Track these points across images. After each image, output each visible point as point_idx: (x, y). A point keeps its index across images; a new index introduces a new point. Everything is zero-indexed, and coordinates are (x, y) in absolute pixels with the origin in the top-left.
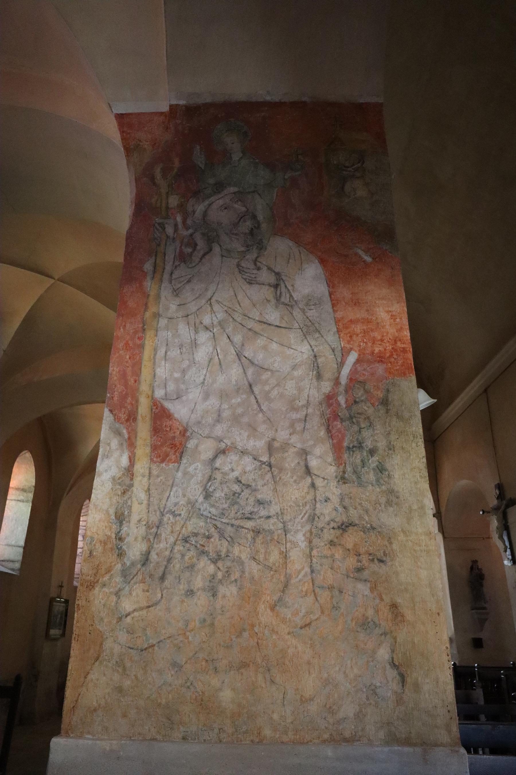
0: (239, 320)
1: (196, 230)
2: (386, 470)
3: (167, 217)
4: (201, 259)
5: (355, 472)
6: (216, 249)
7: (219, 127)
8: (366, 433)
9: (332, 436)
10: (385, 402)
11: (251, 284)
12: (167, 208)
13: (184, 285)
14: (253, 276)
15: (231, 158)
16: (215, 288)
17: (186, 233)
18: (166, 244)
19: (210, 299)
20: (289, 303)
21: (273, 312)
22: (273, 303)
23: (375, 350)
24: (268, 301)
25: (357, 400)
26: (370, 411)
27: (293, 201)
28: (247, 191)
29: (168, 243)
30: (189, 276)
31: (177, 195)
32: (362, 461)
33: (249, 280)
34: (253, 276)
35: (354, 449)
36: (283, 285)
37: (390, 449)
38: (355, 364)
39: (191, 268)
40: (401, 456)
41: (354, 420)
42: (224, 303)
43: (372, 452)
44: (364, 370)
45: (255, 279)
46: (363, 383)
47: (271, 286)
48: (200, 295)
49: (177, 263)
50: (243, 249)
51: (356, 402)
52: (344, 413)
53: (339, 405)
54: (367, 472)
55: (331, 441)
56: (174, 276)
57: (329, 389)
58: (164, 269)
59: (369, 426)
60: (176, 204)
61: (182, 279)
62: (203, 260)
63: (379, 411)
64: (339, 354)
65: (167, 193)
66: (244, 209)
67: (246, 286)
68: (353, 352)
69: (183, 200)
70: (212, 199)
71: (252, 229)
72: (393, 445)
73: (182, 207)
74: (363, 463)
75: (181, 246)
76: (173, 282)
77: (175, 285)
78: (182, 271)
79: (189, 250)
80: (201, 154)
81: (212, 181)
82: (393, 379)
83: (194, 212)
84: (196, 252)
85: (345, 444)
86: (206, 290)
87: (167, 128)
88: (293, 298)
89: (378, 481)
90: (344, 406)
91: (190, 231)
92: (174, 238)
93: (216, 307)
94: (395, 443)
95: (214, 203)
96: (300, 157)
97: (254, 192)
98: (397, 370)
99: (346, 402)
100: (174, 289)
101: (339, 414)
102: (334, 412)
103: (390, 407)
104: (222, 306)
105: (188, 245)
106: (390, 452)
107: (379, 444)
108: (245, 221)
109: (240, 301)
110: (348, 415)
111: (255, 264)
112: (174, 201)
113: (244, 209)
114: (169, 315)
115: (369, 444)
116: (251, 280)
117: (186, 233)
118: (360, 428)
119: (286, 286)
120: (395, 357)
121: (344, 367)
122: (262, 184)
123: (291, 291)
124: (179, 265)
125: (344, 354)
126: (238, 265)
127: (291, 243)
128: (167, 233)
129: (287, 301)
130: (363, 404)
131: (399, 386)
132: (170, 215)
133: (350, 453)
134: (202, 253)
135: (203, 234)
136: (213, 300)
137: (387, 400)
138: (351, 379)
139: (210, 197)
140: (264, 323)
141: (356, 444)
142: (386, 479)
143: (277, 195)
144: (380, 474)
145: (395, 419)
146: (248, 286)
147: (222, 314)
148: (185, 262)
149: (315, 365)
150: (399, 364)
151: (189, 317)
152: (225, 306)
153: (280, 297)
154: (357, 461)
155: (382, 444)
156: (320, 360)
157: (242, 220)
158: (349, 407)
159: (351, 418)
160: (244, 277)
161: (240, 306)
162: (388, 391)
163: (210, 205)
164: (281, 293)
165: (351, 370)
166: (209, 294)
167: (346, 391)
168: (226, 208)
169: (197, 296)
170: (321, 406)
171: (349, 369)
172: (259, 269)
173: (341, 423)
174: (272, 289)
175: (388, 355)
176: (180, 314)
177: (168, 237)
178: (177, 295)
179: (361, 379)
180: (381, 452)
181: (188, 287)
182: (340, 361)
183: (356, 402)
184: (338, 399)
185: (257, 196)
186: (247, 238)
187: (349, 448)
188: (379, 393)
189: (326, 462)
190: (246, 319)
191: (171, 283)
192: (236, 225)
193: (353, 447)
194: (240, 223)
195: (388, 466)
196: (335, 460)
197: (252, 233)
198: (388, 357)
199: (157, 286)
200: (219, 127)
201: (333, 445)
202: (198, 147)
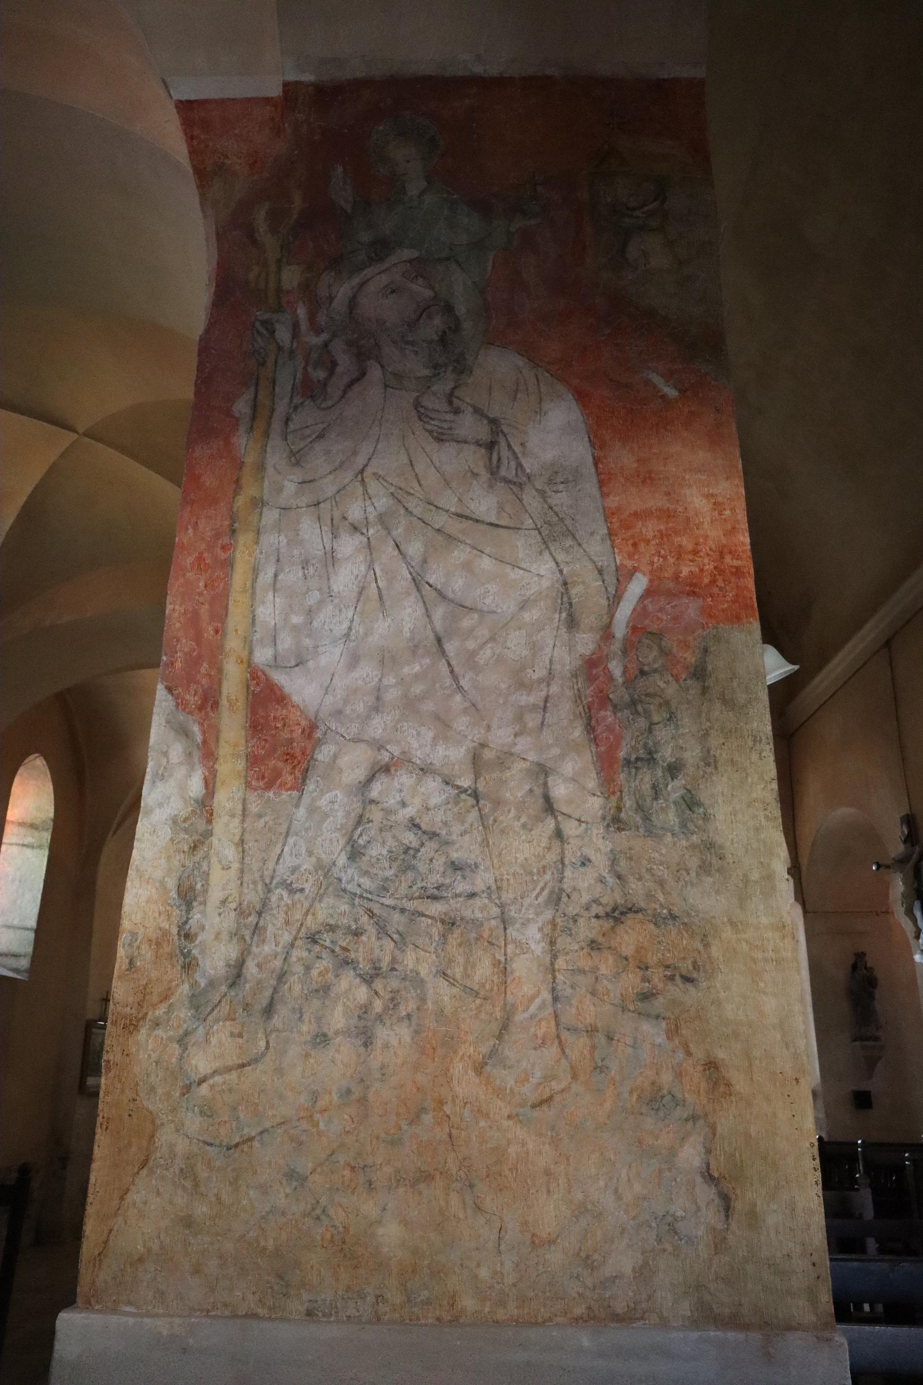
0: (417, 511)
1: (334, 335)
2: (699, 804)
3: (279, 309)
4: (345, 392)
5: (639, 808)
6: (375, 373)
8: (662, 734)
9: (595, 738)
10: (699, 673)
11: (442, 440)
12: (279, 290)
13: (311, 442)
14: (446, 426)
16: (371, 450)
17: (316, 340)
18: (276, 362)
19: (362, 472)
23: (681, 572)
25: (646, 668)
26: (671, 691)
28: (436, 257)
29: (280, 362)
30: (321, 426)
31: (298, 264)
32: (654, 787)
34: (446, 426)
35: (639, 764)
36: (503, 444)
37: (708, 764)
38: (643, 598)
39: (324, 409)
40: (729, 779)
41: (640, 708)
43: (674, 770)
44: (661, 610)
46: (656, 636)
47: (480, 445)
48: (342, 463)
49: (297, 400)
50: (427, 372)
51: (642, 673)
52: (619, 694)
53: (611, 678)
54: (662, 808)
55: (594, 750)
56: (292, 426)
57: (591, 647)
59: (669, 720)
60: (295, 284)
61: (308, 431)
62: (350, 394)
63: (688, 689)
64: (611, 580)
65: (279, 261)
66: (429, 293)
67: (431, 446)
68: (638, 575)
70: (368, 272)
71: (444, 332)
72: (714, 756)
73: (307, 289)
74: (656, 791)
75: (305, 368)
76: (290, 437)
79: (321, 374)
81: (366, 237)
82: (717, 628)
83: (331, 299)
85: (622, 754)
86: (355, 453)
88: (523, 470)
89: (683, 825)
90: (620, 680)
91: (325, 336)
94: (719, 752)
96: (539, 188)
97: (448, 259)
98: (723, 610)
99: (624, 672)
101: (611, 696)
102: (602, 691)
103: (710, 682)
104: (385, 484)
106: (709, 770)
107: (687, 755)
108: (430, 317)
110: (627, 698)
111: (450, 403)
112: (291, 277)
113: (429, 293)
114: (282, 502)
115: (667, 754)
117: (316, 340)
118: (652, 724)
119: (509, 446)
120: (720, 583)
121: (621, 604)
123: (520, 455)
124: (302, 403)
125: (620, 578)
126: (417, 405)
127: (520, 362)
128: (279, 341)
129: (511, 475)
130: (657, 676)
131: (728, 642)
133: (630, 773)
134: (346, 380)
135: (349, 343)
136: (369, 471)
137: (704, 669)
138: (634, 629)
139: (362, 269)
141: (642, 753)
142: (700, 822)
143: (493, 267)
144: (688, 812)
145: (718, 705)
146: (435, 445)
147: (385, 500)
149: (565, 599)
150: (728, 599)
151: (321, 505)
153: (498, 467)
154: (643, 787)
155: (692, 755)
156: (574, 591)
158: (629, 683)
159: (633, 703)
160: (429, 427)
161: (420, 485)
162: (706, 651)
163: (362, 284)
164: (499, 459)
165: (634, 609)
166: (360, 461)
167: (625, 652)
168: (393, 292)
169: (337, 464)
170: (574, 680)
171: (632, 608)
172: (457, 412)
173: (615, 713)
175: (706, 580)
177: (280, 348)
178: (298, 463)
179: (654, 627)
180: (690, 770)
181: (318, 447)
182: (613, 592)
183: (642, 673)
184: (610, 666)
187: (628, 762)
188: (687, 655)
189: (584, 788)
190: (431, 511)
191: (286, 439)
192: (412, 325)
193: (637, 759)
194: (422, 321)
195: (703, 796)
196: (601, 785)
197: (443, 340)
198: (706, 586)
200: (381, 128)
201: (599, 755)
202: (340, 169)
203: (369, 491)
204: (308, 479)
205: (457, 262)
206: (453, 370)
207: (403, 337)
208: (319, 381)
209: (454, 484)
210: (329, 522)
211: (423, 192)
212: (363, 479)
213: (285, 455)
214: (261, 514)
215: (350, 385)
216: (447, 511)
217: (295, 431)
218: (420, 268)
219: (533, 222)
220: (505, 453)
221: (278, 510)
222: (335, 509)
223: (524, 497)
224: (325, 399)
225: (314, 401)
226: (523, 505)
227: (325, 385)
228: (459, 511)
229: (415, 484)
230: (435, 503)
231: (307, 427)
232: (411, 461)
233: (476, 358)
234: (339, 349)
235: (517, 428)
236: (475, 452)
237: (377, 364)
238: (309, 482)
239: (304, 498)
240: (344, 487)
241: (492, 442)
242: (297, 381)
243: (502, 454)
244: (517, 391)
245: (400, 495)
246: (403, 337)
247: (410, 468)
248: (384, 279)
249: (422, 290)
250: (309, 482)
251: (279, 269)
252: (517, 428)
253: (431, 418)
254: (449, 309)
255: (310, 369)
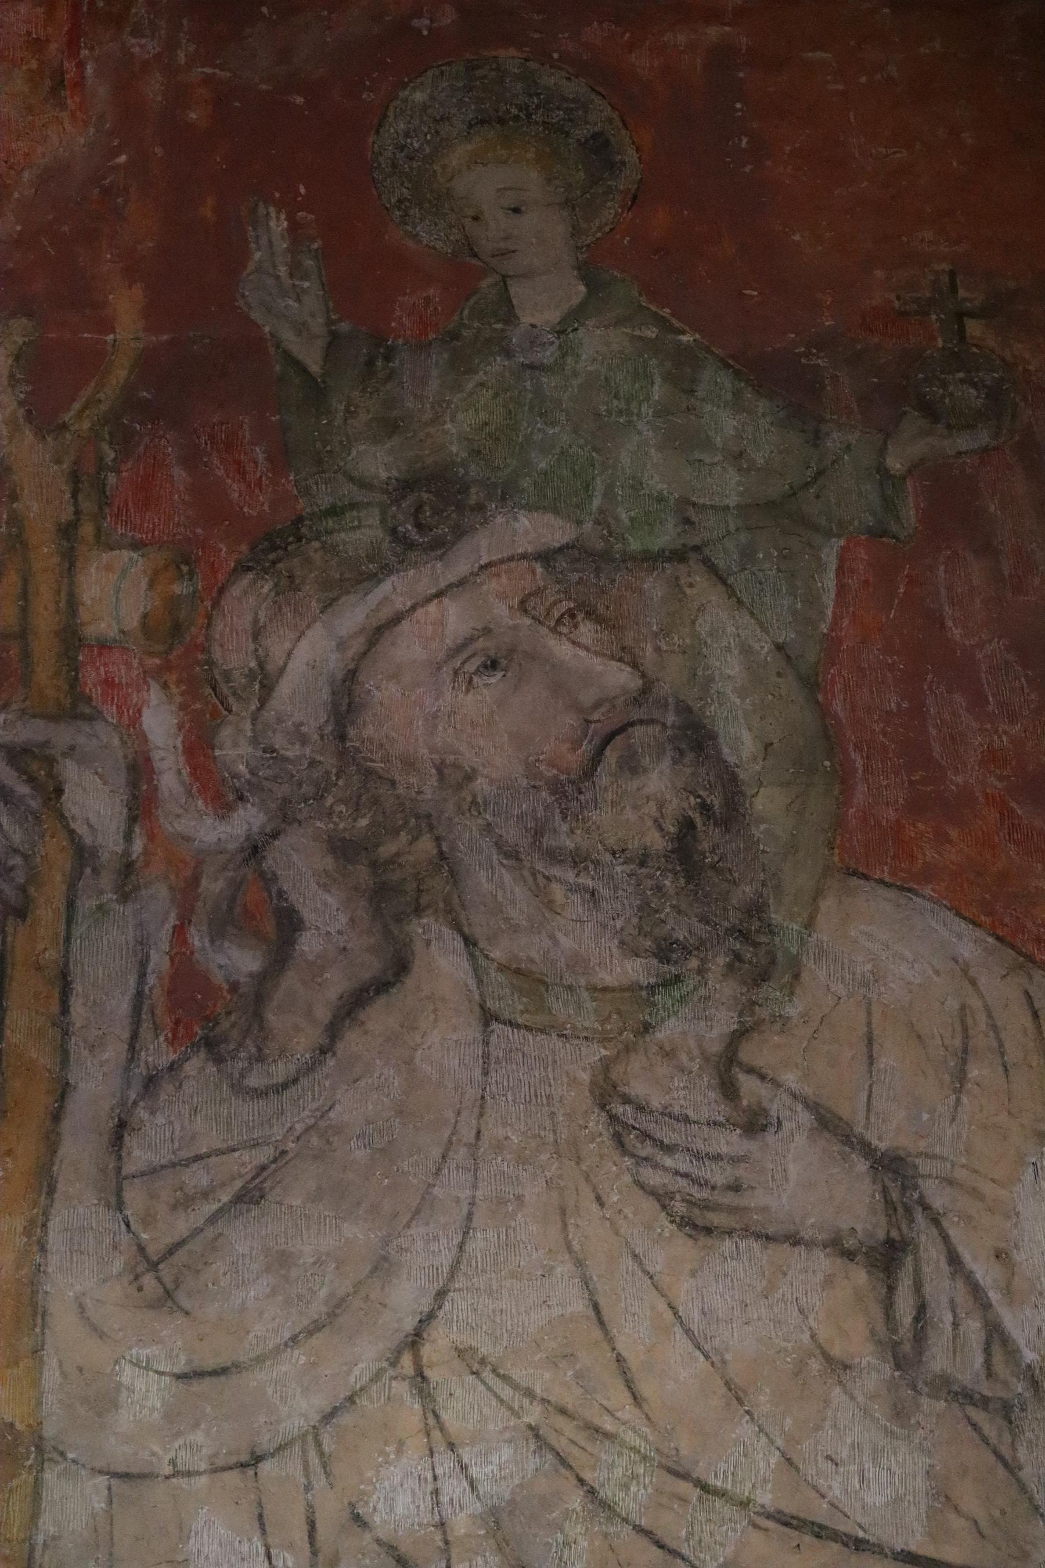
0: (633, 1501)
1: (285, 817)
3: (75, 708)
4: (334, 1031)
6: (442, 963)
7: (419, 97)
11: (708, 1231)
12: (71, 639)
13: (212, 1220)
14: (718, 1174)
15: (506, 311)
16: (445, 1260)
18: (71, 905)
19: (415, 1340)
20: (985, 1389)
21: (876, 1452)
22: (871, 1382)
24: (839, 1367)
27: (957, 632)
28: (635, 545)
29: (86, 904)
30: (251, 1159)
31: (135, 546)
33: (691, 1203)
34: (718, 1174)
36: (931, 1253)
39: (260, 1094)
42: (517, 1374)
45: (728, 1199)
47: (849, 1255)
48: (337, 1306)
49: (157, 1053)
50: (636, 970)
56: (139, 1155)
58: (63, 1091)
60: (132, 622)
61: (197, 1178)
62: (352, 1041)
65: (68, 531)
66: (620, 677)
67: (669, 1250)
69: (179, 588)
70: (393, 591)
71: (687, 825)
73: (176, 642)
75: (179, 932)
76: (134, 1196)
77: (148, 1220)
78: (197, 1117)
79: (242, 960)
80: (296, 269)
81: (378, 462)
83: (264, 679)
84: (290, 980)
86: (383, 1266)
87: (58, 85)
88: (1012, 1352)
91: (248, 819)
92: (127, 868)
93: (464, 1404)
95: (405, 625)
96: (974, 328)
97: (679, 556)
100: (142, 1249)
104: (506, 1392)
105: (231, 921)
108: (630, 765)
109: (634, 1360)
111: (729, 1090)
112: (116, 592)
113: (620, 677)
114: (120, 1454)
116: (706, 1206)
119: (954, 1259)
122: (732, 501)
123: (994, 1296)
126: (606, 1092)
127: (969, 944)
128: (81, 829)
129: (969, 1369)
132: (96, 693)
134: (336, 984)
135: (344, 849)
136: (438, 1345)
139: (374, 578)
140: (821, 1532)
143: (842, 590)
146: (683, 1246)
147: (507, 1452)
148: (212, 1047)
151: (266, 1467)
152: (529, 1393)
153: (920, 1337)
157: (611, 756)
160: (654, 1178)
161: (637, 1399)
163: (378, 633)
164: (921, 1309)
166: (406, 1297)
168: (492, 665)
169: (317, 1309)
172: (755, 1123)
174: (860, 1276)
176: (201, 1444)
177: (83, 855)
178: (167, 1299)
181: (244, 1239)
185: (700, 585)
186: (659, 888)
190: (684, 1500)
191: (120, 1206)
192: (570, 789)
194: (603, 778)
199: (19, 1223)
200: (419, 97)
202: (278, 224)
203: (445, 1416)
204: (210, 1364)
205: (712, 569)
206: (730, 967)
207: (538, 833)
208: (234, 987)
209: (763, 1401)
210: (300, 1535)
211: (576, 315)
212: (420, 1374)
213: (118, 1265)
214: (36, 1496)
215: (355, 1003)
216: (745, 1504)
217: (153, 1171)
218: (585, 579)
219: (964, 442)
220: (940, 1287)
221: (102, 1480)
222: (320, 1482)
223: (1022, 1454)
224: (260, 1058)
225: (219, 1060)
226: (1023, 1488)
227: (260, 999)
228: (789, 1508)
229: (619, 1397)
230: (698, 1472)
231: (198, 1158)
232: (596, 1307)
233: (809, 925)
234: (301, 866)
235: (975, 1194)
236: (829, 1281)
237: (446, 931)
238: (215, 1373)
239: (198, 1437)
240: (351, 1399)
241: (890, 1242)
242: (151, 980)
243: (928, 1289)
244: (964, 1054)
245: (565, 1434)
246: (538, 833)
247: (597, 1334)
248: (455, 618)
249: (597, 664)
250: (215, 1373)
251: (70, 561)
252: (975, 1194)
253: (686, 1175)
254: (696, 739)
255: (197, 939)
